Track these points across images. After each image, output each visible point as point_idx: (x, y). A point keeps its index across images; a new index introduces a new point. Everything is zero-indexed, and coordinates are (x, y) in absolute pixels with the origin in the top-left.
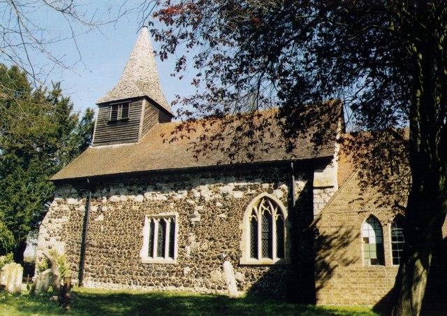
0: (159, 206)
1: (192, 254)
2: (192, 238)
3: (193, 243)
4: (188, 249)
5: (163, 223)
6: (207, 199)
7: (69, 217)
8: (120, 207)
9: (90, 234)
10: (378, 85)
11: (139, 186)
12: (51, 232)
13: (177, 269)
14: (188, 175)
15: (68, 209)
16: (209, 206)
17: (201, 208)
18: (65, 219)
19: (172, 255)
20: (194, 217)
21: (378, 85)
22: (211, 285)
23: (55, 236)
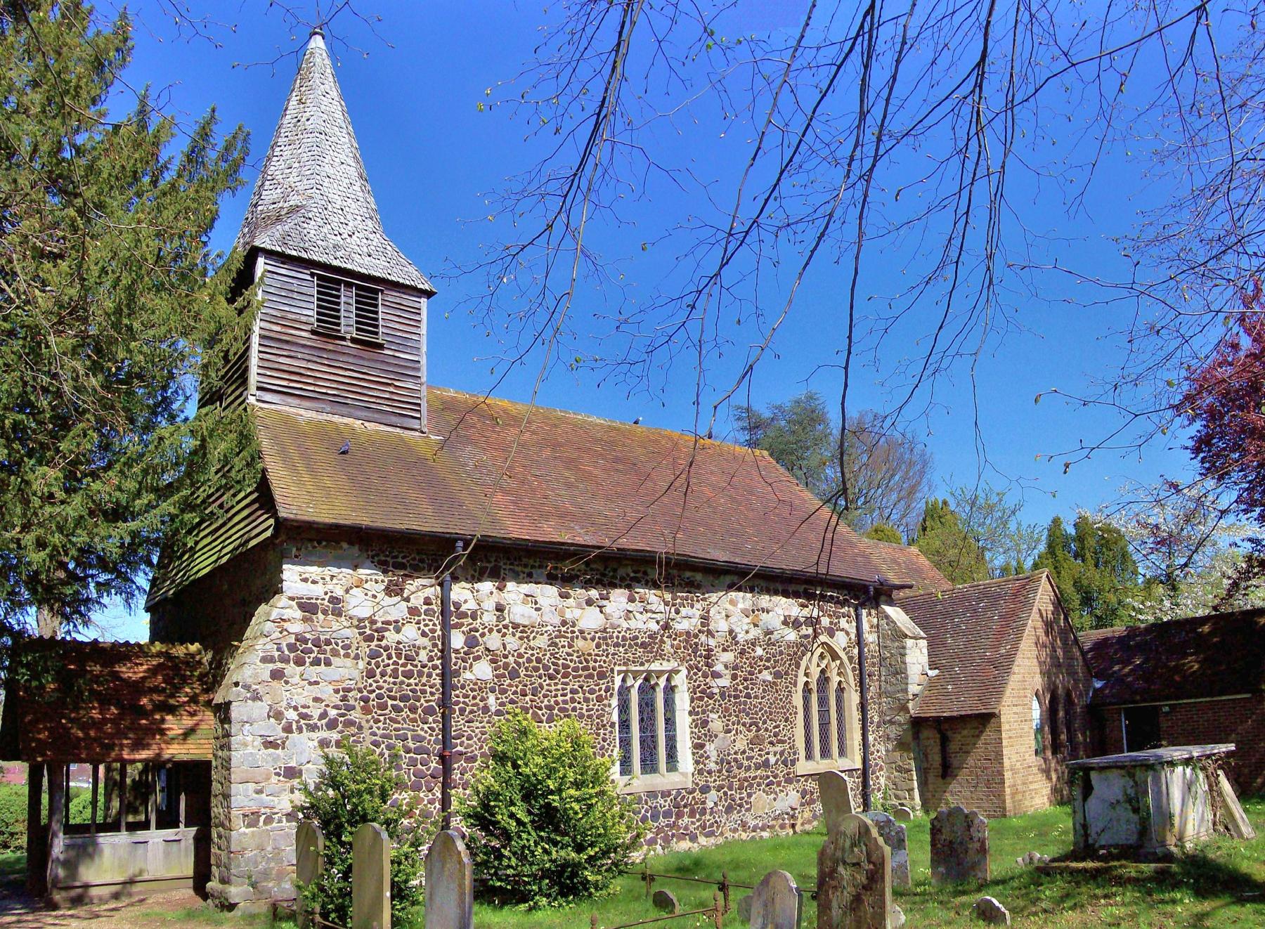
0: (643, 645)
1: (720, 762)
2: (716, 724)
3: (721, 735)
4: (711, 748)
5: (647, 689)
6: (741, 637)
7: (362, 665)
8: (542, 642)
9: (458, 723)
10: (103, 577)
11: (587, 585)
12: (292, 715)
13: (694, 798)
14: (699, 577)
15: (353, 633)
16: (742, 653)
17: (728, 657)
18: (346, 670)
19: (842, 752)
20: (716, 675)
21: (103, 577)
22: (752, 823)
23: (313, 728)
